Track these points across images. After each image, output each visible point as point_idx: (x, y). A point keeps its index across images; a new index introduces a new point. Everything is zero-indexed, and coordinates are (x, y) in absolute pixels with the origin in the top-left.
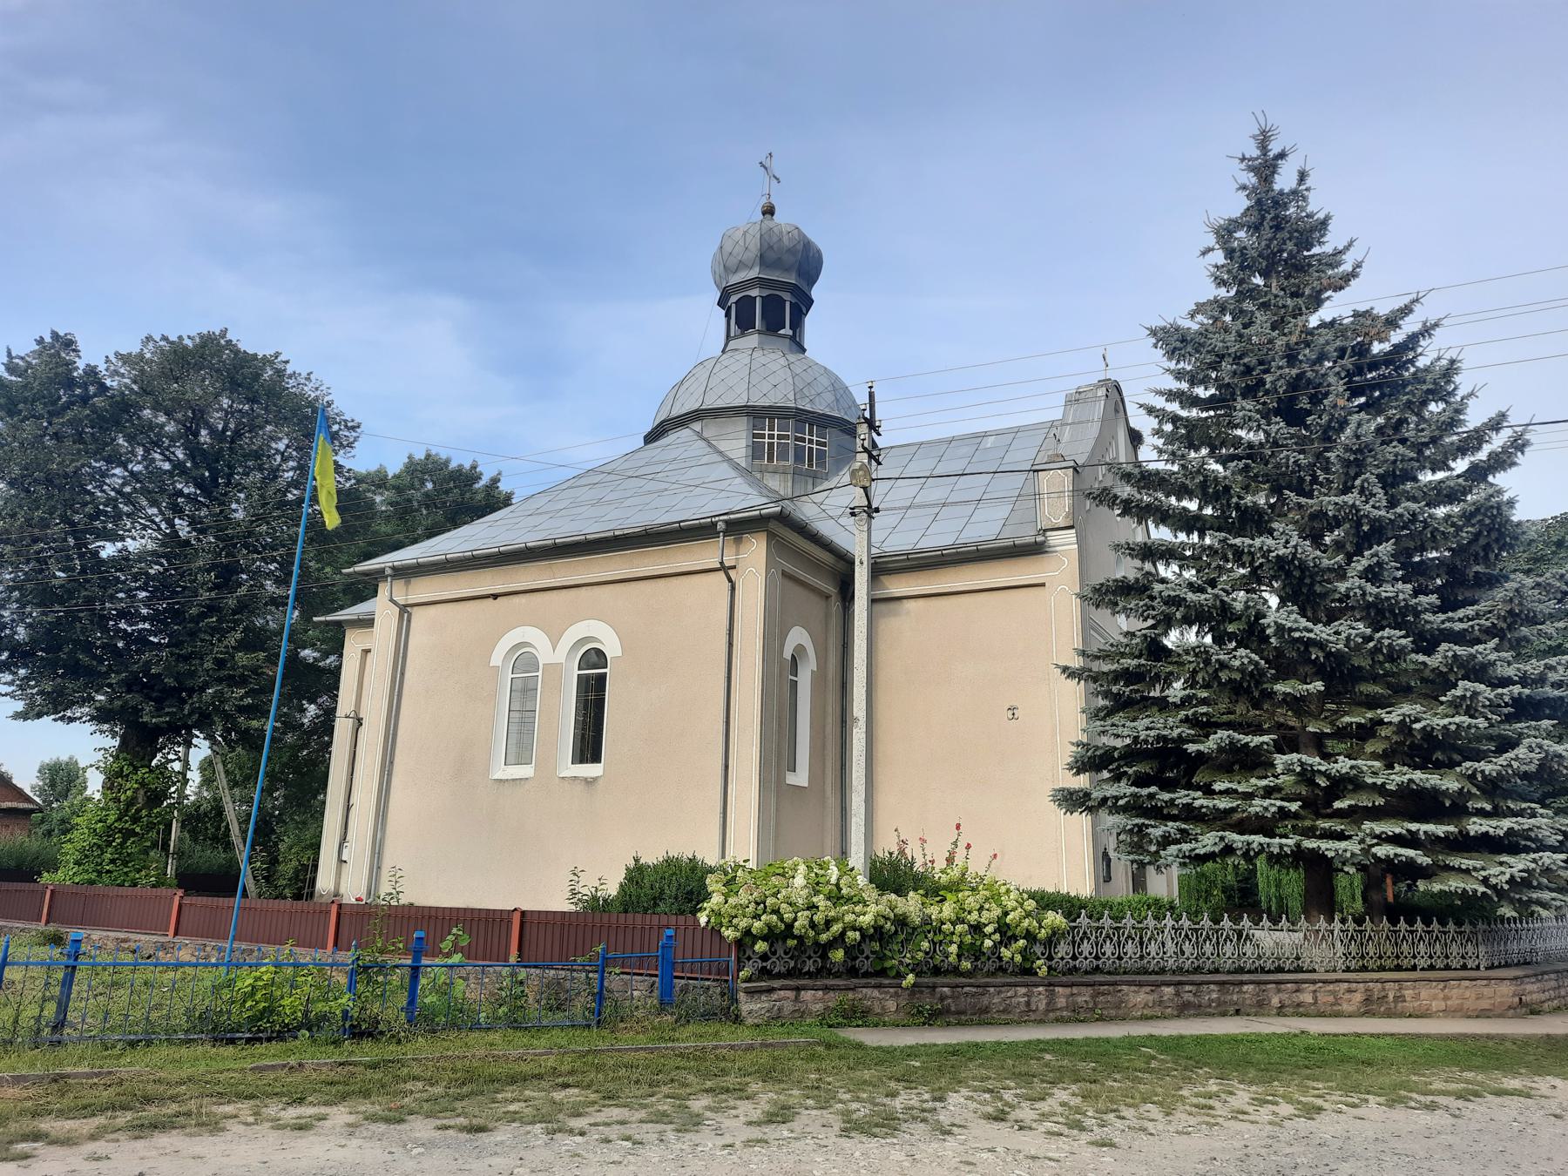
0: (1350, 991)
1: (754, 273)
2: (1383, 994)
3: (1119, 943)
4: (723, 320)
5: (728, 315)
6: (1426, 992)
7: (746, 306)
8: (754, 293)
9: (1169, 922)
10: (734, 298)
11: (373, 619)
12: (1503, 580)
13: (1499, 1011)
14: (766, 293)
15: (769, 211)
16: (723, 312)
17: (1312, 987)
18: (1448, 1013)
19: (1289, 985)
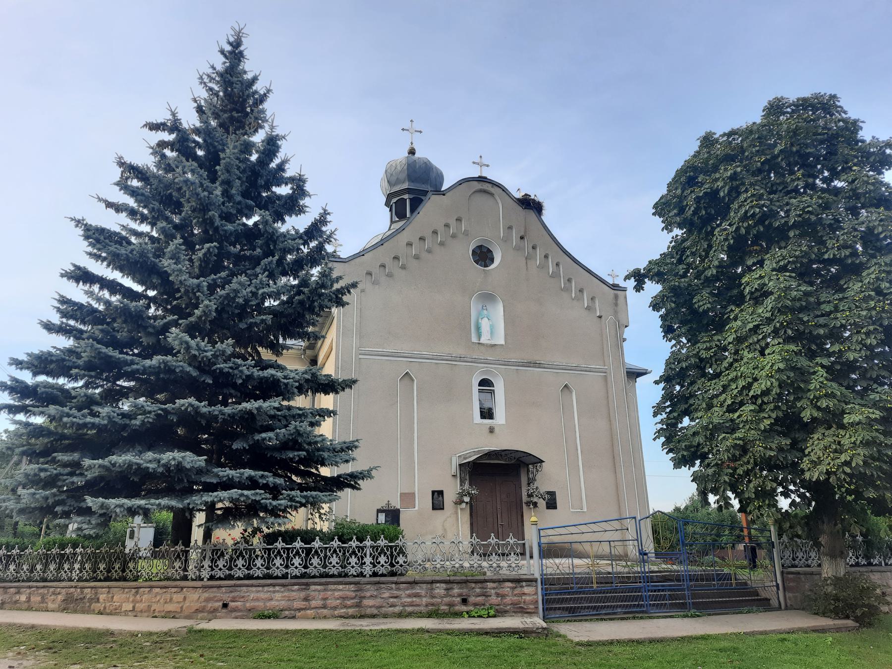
0: (54, 593)
1: (406, 186)
2: (82, 596)
3: (806, 551)
4: (389, 214)
5: (391, 210)
6: (118, 596)
7: (401, 204)
8: (406, 196)
9: (368, 543)
10: (394, 200)
11: (480, 385)
12: (305, 324)
13: (186, 613)
14: (412, 196)
15: (412, 152)
16: (388, 209)
17: (28, 591)
18: (135, 613)
19: (12, 589)
